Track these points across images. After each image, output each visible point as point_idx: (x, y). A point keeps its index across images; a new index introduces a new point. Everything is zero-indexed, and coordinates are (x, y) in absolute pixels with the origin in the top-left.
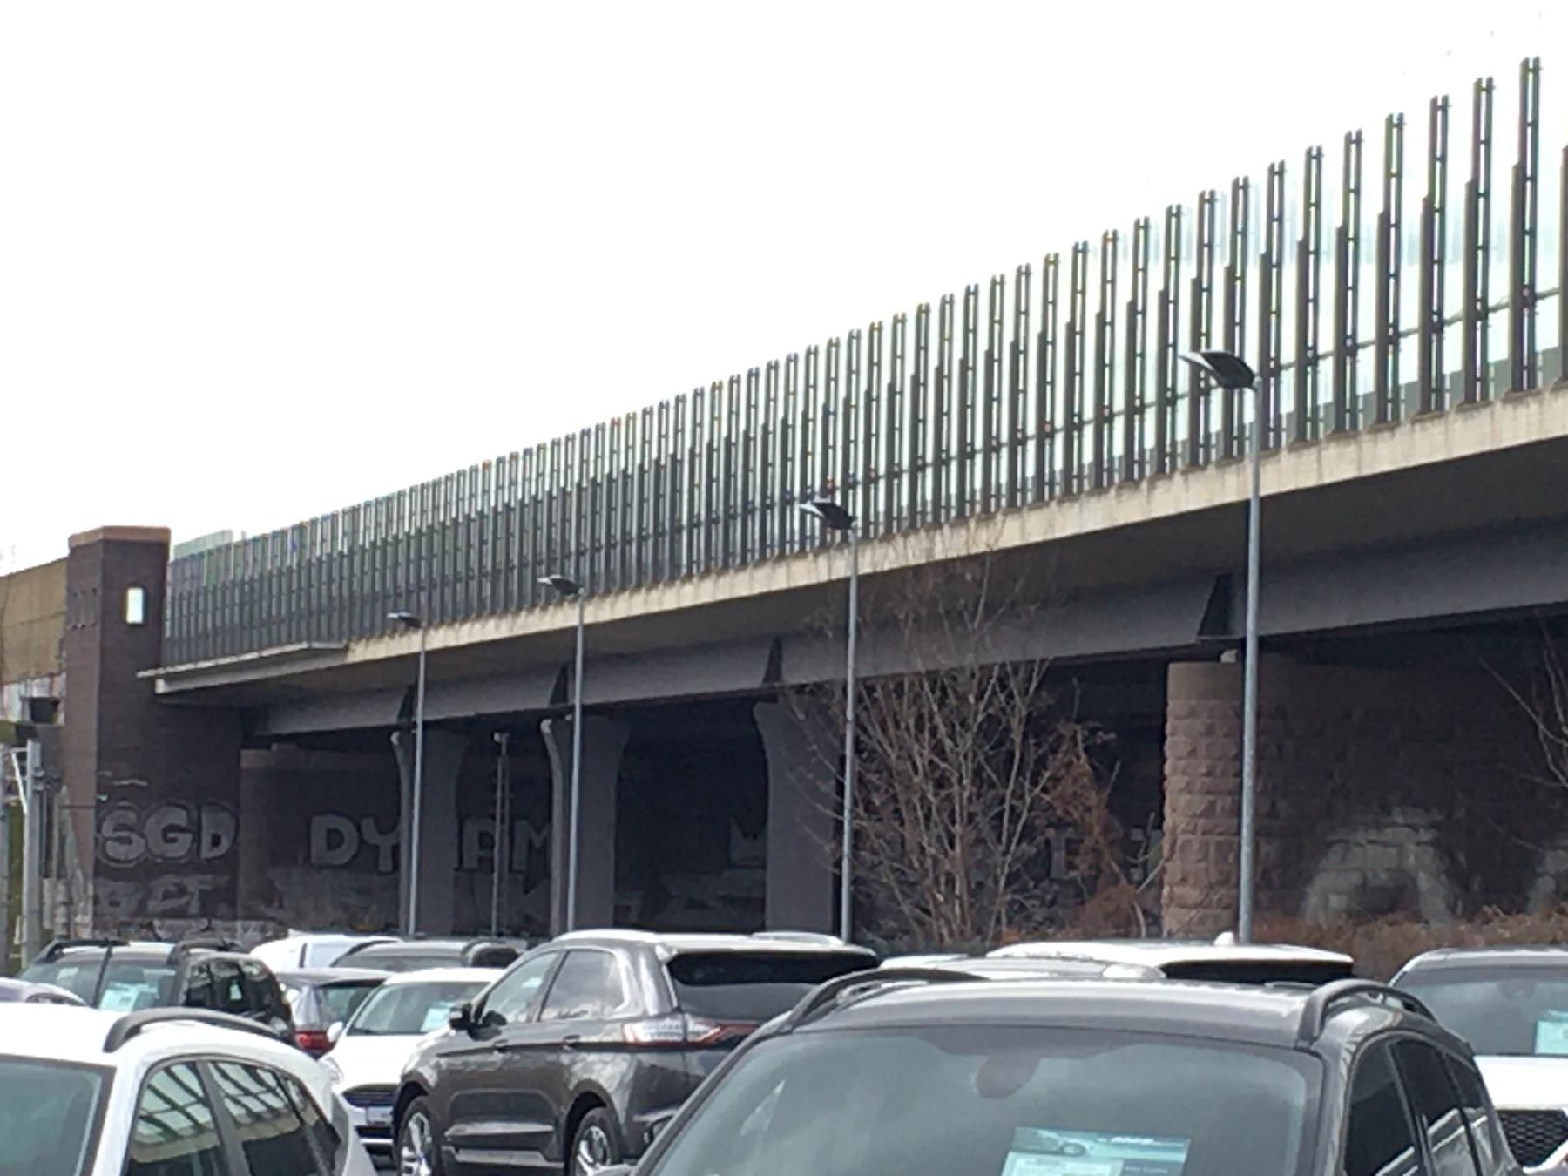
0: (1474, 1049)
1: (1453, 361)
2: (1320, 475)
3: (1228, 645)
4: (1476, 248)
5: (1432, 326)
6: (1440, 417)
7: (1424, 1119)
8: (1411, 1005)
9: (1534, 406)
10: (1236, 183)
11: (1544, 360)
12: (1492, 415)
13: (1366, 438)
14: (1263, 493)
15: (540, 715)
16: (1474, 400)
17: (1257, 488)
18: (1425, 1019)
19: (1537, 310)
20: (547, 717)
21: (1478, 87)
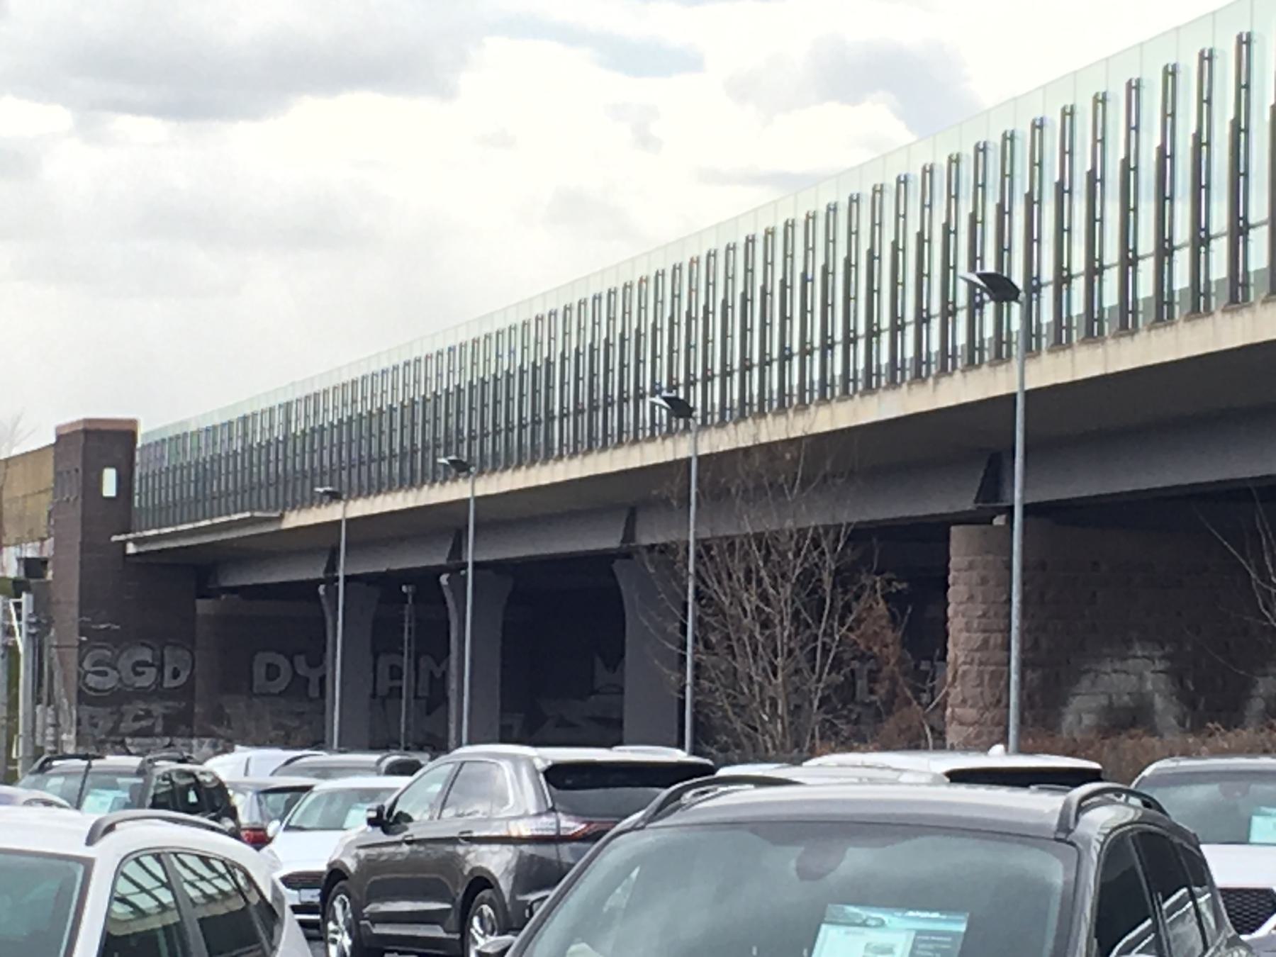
0: (1200, 839)
3: (1000, 511)
6: (1171, 324)
8: (1148, 803)
10: (1129, 83)
11: (1217, 288)
13: (1110, 342)
14: (1028, 387)
17: (1022, 384)
20: (322, 583)
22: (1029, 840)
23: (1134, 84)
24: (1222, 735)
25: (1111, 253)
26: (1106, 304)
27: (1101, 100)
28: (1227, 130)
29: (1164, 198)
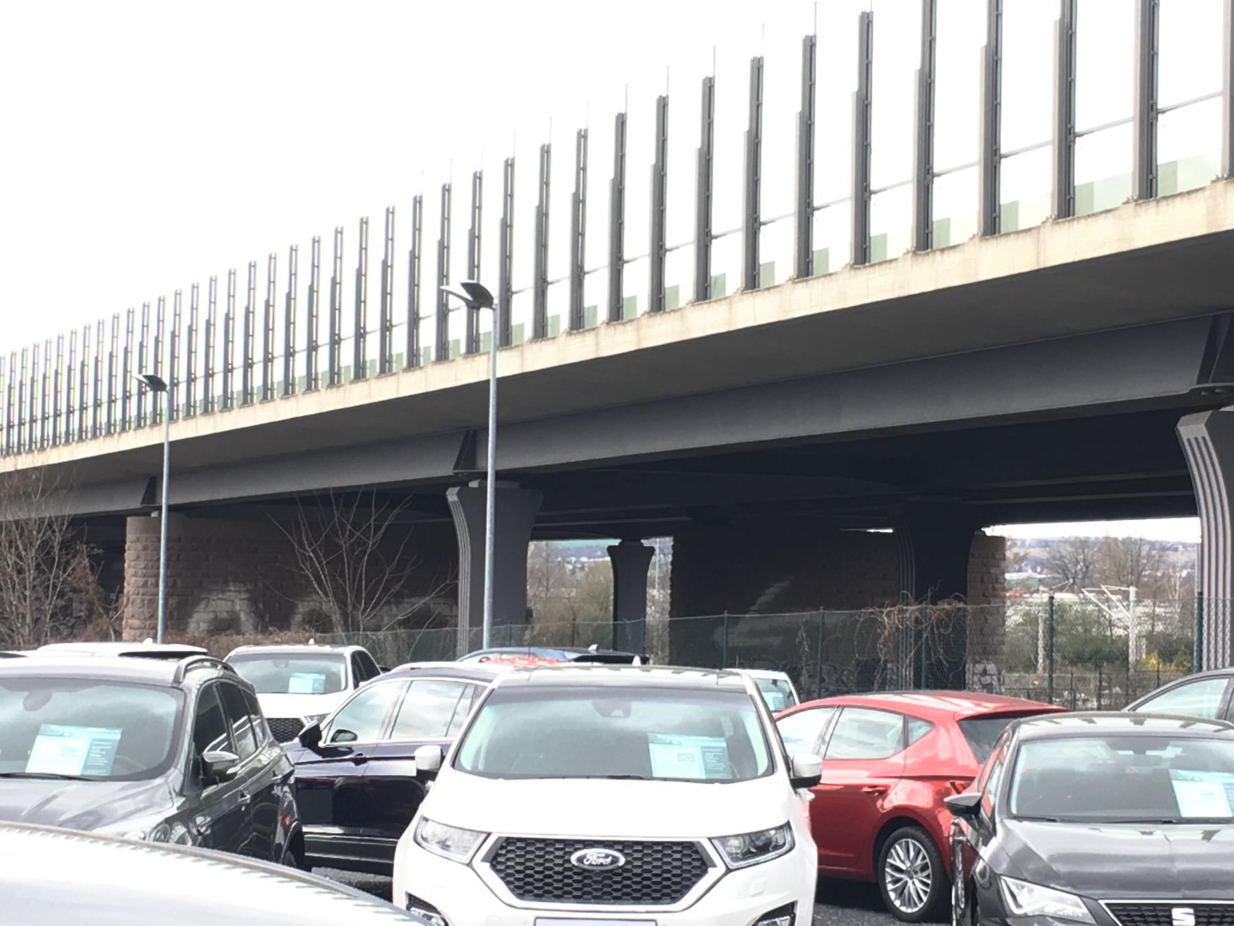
15: (445, 483)
18: (231, 673)
20: (454, 485)
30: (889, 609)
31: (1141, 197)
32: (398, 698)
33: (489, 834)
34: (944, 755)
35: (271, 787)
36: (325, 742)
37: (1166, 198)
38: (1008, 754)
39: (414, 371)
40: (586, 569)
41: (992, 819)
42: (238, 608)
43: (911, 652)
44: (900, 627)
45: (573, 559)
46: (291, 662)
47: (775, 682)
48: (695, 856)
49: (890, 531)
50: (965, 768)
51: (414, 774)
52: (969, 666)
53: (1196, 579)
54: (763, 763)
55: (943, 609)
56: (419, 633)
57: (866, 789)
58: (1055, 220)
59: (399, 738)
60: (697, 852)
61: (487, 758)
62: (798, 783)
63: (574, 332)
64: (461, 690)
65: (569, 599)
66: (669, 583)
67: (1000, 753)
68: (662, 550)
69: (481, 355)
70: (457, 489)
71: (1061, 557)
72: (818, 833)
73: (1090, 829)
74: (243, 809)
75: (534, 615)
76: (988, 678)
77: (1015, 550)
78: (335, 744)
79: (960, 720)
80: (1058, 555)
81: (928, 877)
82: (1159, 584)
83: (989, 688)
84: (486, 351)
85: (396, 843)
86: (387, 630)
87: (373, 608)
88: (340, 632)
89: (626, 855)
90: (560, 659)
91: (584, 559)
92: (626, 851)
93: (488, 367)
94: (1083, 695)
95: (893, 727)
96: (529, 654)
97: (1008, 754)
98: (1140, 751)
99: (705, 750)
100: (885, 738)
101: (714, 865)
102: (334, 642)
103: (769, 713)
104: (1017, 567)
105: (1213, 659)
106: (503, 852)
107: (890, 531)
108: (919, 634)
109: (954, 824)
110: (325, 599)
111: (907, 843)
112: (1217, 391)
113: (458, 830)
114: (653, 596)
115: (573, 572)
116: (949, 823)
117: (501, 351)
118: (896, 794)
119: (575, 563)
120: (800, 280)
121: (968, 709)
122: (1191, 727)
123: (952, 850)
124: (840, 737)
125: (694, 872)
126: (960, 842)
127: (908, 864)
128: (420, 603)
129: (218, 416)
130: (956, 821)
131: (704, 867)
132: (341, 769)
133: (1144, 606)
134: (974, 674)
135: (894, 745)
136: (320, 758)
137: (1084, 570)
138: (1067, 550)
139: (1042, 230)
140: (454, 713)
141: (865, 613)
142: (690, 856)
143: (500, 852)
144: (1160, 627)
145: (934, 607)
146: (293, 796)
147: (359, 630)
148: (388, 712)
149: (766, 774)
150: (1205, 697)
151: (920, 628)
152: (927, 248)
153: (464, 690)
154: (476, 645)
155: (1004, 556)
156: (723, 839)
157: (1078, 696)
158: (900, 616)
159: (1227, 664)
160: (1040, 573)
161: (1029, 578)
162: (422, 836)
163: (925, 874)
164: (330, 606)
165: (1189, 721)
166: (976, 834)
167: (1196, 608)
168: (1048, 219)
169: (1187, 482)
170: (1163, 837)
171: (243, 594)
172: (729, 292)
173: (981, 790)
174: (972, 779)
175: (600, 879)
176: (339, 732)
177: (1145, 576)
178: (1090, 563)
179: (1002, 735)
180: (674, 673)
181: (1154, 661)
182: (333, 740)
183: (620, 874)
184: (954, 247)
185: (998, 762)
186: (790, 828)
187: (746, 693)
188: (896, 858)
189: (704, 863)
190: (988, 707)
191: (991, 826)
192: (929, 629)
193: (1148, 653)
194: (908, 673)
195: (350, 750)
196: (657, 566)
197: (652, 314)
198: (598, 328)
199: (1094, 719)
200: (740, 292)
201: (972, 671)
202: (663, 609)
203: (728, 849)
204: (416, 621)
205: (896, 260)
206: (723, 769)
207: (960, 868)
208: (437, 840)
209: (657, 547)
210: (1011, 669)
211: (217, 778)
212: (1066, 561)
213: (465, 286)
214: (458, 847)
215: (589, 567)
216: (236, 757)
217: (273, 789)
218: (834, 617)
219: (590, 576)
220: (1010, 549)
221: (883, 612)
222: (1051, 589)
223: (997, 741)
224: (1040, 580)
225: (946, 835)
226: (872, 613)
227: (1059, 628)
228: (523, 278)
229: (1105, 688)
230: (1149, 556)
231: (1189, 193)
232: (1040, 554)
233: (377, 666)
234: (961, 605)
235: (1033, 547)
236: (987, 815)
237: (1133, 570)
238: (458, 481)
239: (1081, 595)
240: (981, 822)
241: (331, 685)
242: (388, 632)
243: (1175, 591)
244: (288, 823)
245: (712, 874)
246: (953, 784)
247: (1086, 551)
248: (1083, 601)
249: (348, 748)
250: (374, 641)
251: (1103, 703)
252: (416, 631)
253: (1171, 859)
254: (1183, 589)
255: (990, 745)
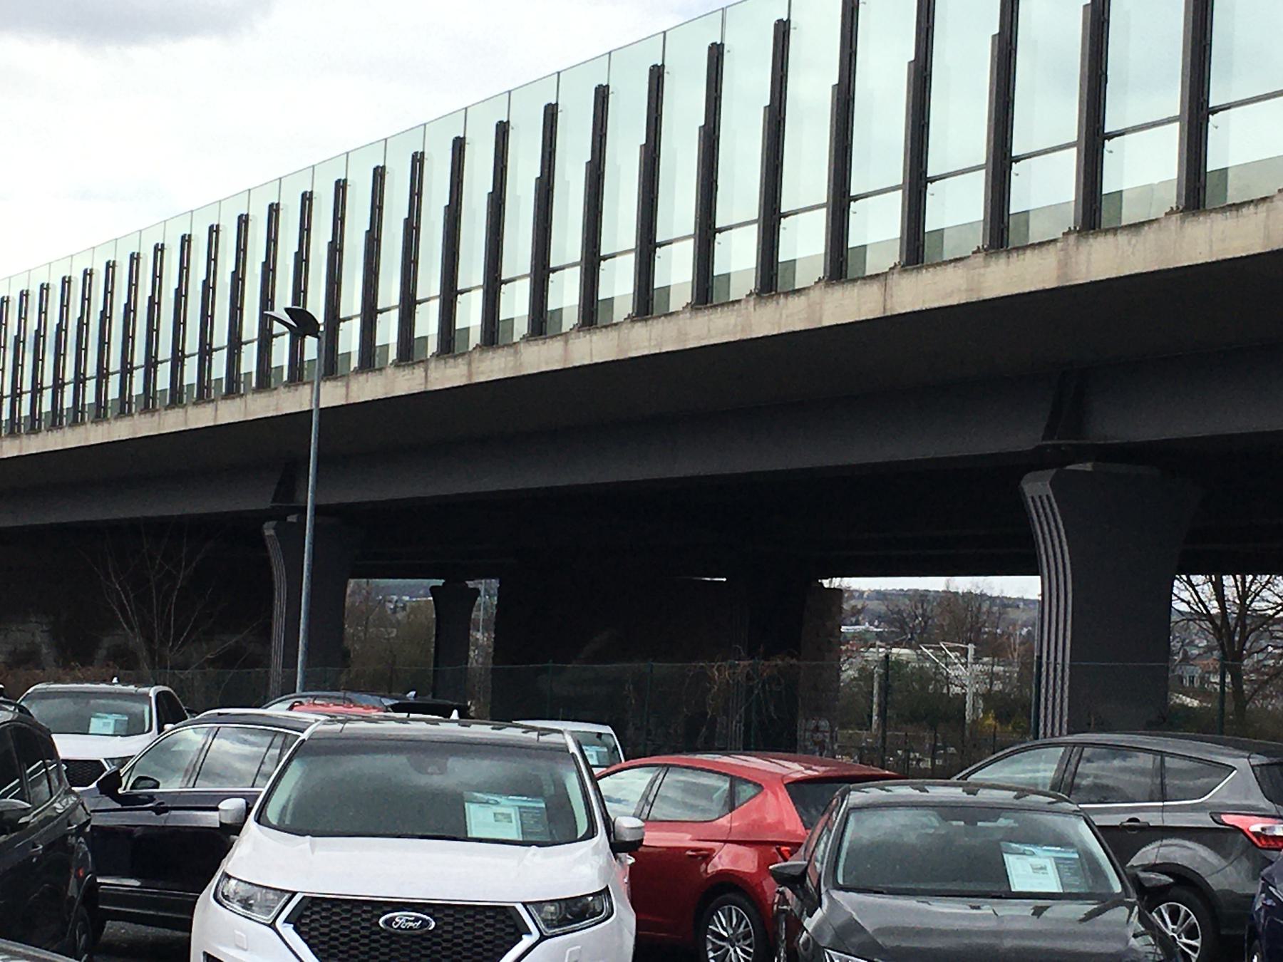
0: (52, 730)
1: (68, 402)
2: (186, 422)
3: (293, 510)
4: (104, 343)
5: (58, 385)
6: (61, 428)
7: (25, 765)
8: (22, 709)
9: (106, 425)
10: (22, 292)
11: (245, 378)
12: (64, 433)
13: (89, 425)
14: (322, 406)
15: (263, 516)
16: (124, 413)
17: (318, 404)
18: (27, 716)
19: (134, 374)
20: (270, 518)
21: (156, 247)
22: (958, 894)
23: (25, 293)
24: (79, 670)
25: (91, 370)
26: (23, 414)
27: (159, 250)
28: (172, 295)
29: (59, 355)
30: (719, 663)
31: (991, 246)
32: (204, 745)
33: (294, 894)
34: (771, 818)
35: (65, 836)
36: (124, 789)
37: (1017, 249)
38: (837, 819)
39: (234, 398)
40: (408, 609)
41: (818, 888)
42: (38, 639)
43: (741, 708)
44: (731, 682)
45: (395, 598)
46: (92, 702)
47: (599, 735)
48: (508, 922)
49: (724, 580)
50: (794, 834)
51: (218, 826)
52: (801, 722)
53: (1036, 638)
54: (582, 828)
55: (776, 665)
56: (230, 673)
57: (689, 853)
58: (902, 267)
59: (203, 787)
60: (510, 917)
61: (293, 814)
62: (617, 846)
63: (403, 364)
64: (270, 739)
65: (388, 639)
66: (492, 627)
67: (829, 818)
68: (487, 592)
69: (304, 384)
70: (273, 523)
71: (900, 612)
72: (637, 900)
73: (918, 902)
74: (34, 860)
75: (352, 656)
76: (820, 735)
77: (853, 602)
78: (135, 791)
79: (789, 783)
80: (896, 609)
81: (749, 946)
82: (999, 641)
83: (821, 746)
84: (309, 380)
85: (198, 897)
86: (196, 668)
87: (182, 646)
88: (146, 670)
89: (435, 920)
90: (377, 705)
91: (407, 598)
92: (436, 915)
93: (312, 397)
94: (917, 755)
95: (719, 789)
96: (344, 698)
97: (837, 819)
98: (971, 821)
99: (522, 811)
100: (712, 800)
101: (529, 933)
102: (139, 682)
103: (589, 768)
104: (854, 620)
105: (1049, 725)
106: (308, 913)
107: (724, 580)
108: (750, 691)
109: (778, 892)
110: (131, 635)
111: (730, 910)
112: (1063, 448)
113: (261, 889)
114: (477, 639)
115: (394, 611)
116: (772, 890)
117: (325, 381)
118: (720, 858)
119: (397, 602)
120: (639, 318)
121: (798, 771)
122: (1023, 799)
123: (776, 919)
124: (665, 798)
125: (507, 938)
126: (785, 911)
127: (731, 932)
128: (232, 641)
129: (25, 439)
130: (781, 889)
131: (517, 935)
132: (140, 818)
133: (983, 664)
134: (806, 730)
135: (720, 807)
136: (119, 806)
137: (923, 624)
138: (905, 604)
139: (890, 277)
140: (262, 763)
141: (695, 666)
142: (503, 922)
143: (305, 913)
144: (998, 686)
145: (767, 663)
146: (88, 847)
147: (166, 668)
148: (192, 761)
149: (584, 838)
150: (1041, 766)
151: (751, 684)
152: (771, 291)
153: (273, 740)
154: (287, 689)
155: (841, 608)
156: (538, 905)
157: (912, 755)
158: (732, 671)
159: (1064, 732)
160: (877, 627)
161: (867, 631)
162: (223, 893)
163: (748, 942)
164: (136, 641)
165: (1022, 792)
166: (800, 903)
167: (1033, 671)
168: (895, 265)
169: (1029, 540)
170: (991, 912)
171: (44, 627)
172: (565, 329)
173: (808, 858)
174: (800, 845)
175: (408, 944)
176: (140, 779)
177: (985, 633)
178: (929, 618)
179: (832, 801)
180: (493, 729)
181: (990, 721)
182: (132, 788)
183: (429, 940)
184: (799, 291)
185: (826, 829)
186: (609, 895)
187: (568, 751)
188: (719, 925)
189: (517, 930)
190: (817, 771)
191: (817, 897)
192: (760, 686)
193: (985, 712)
194: (737, 727)
195: (151, 798)
196: (482, 608)
197: (485, 348)
198: (427, 360)
199: (926, 787)
200: (576, 328)
201: (804, 727)
202: (487, 653)
203: (543, 915)
204: (228, 659)
205: (739, 301)
206: (540, 831)
207: (783, 937)
208: (239, 898)
209: (482, 589)
210: (843, 727)
211: (8, 828)
212: (905, 615)
213: (287, 310)
214: (260, 907)
215: (412, 608)
216: (28, 805)
217: (67, 839)
218: (662, 668)
219: (412, 616)
220: (847, 601)
221: (713, 666)
222: (888, 644)
223: (826, 808)
224: (877, 633)
225: (769, 902)
226: (702, 667)
227: (896, 684)
228: (352, 302)
229: (940, 748)
230: (989, 612)
231: (1041, 244)
232: (880, 607)
233: (184, 708)
234: (794, 661)
235: (872, 600)
236: (812, 885)
237: (972, 626)
238: (276, 515)
239: (919, 652)
240: (806, 891)
241: (133, 728)
242: (198, 671)
243: (1015, 650)
244: (81, 874)
245: (526, 941)
246: (779, 850)
247: (925, 606)
248: (921, 657)
249: (149, 796)
250: (181, 680)
251: (937, 763)
252: (228, 670)
253: (997, 934)
254: (1022, 648)
255: (817, 810)
